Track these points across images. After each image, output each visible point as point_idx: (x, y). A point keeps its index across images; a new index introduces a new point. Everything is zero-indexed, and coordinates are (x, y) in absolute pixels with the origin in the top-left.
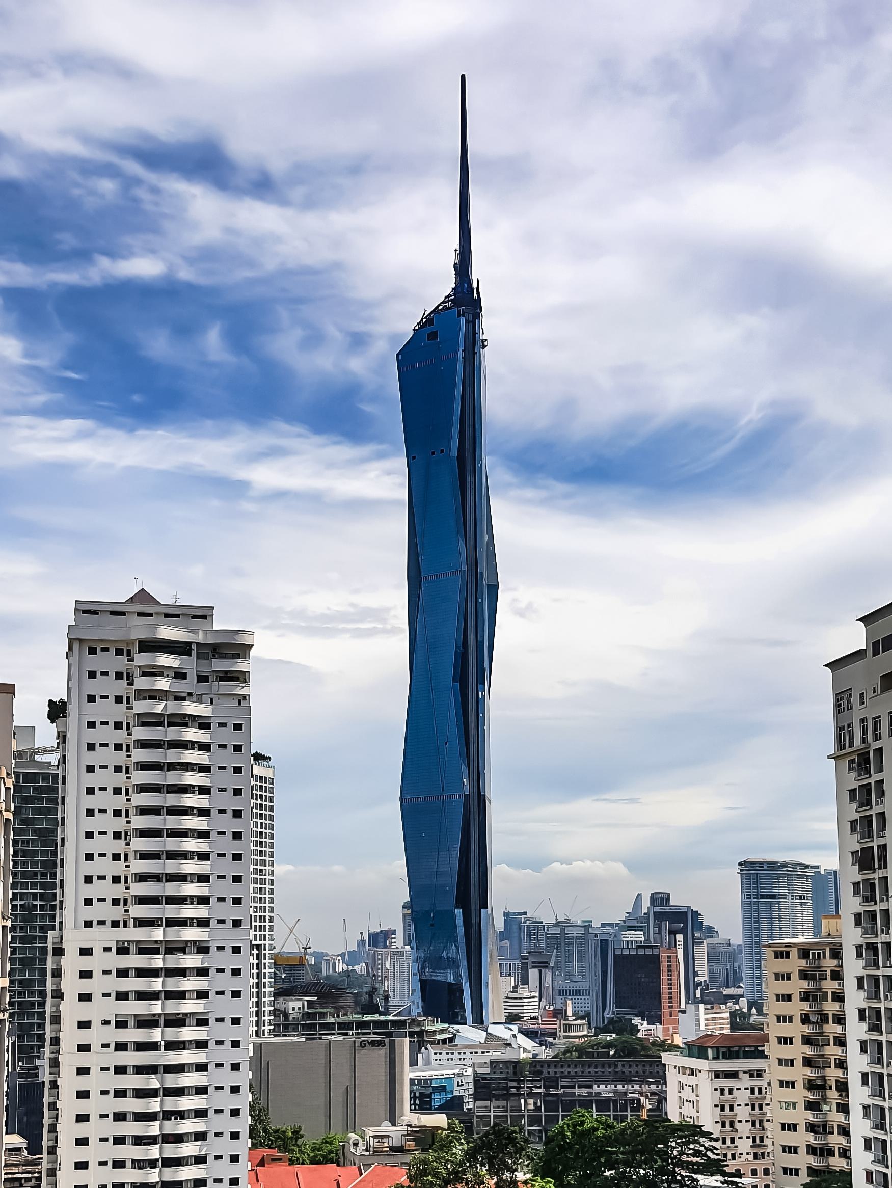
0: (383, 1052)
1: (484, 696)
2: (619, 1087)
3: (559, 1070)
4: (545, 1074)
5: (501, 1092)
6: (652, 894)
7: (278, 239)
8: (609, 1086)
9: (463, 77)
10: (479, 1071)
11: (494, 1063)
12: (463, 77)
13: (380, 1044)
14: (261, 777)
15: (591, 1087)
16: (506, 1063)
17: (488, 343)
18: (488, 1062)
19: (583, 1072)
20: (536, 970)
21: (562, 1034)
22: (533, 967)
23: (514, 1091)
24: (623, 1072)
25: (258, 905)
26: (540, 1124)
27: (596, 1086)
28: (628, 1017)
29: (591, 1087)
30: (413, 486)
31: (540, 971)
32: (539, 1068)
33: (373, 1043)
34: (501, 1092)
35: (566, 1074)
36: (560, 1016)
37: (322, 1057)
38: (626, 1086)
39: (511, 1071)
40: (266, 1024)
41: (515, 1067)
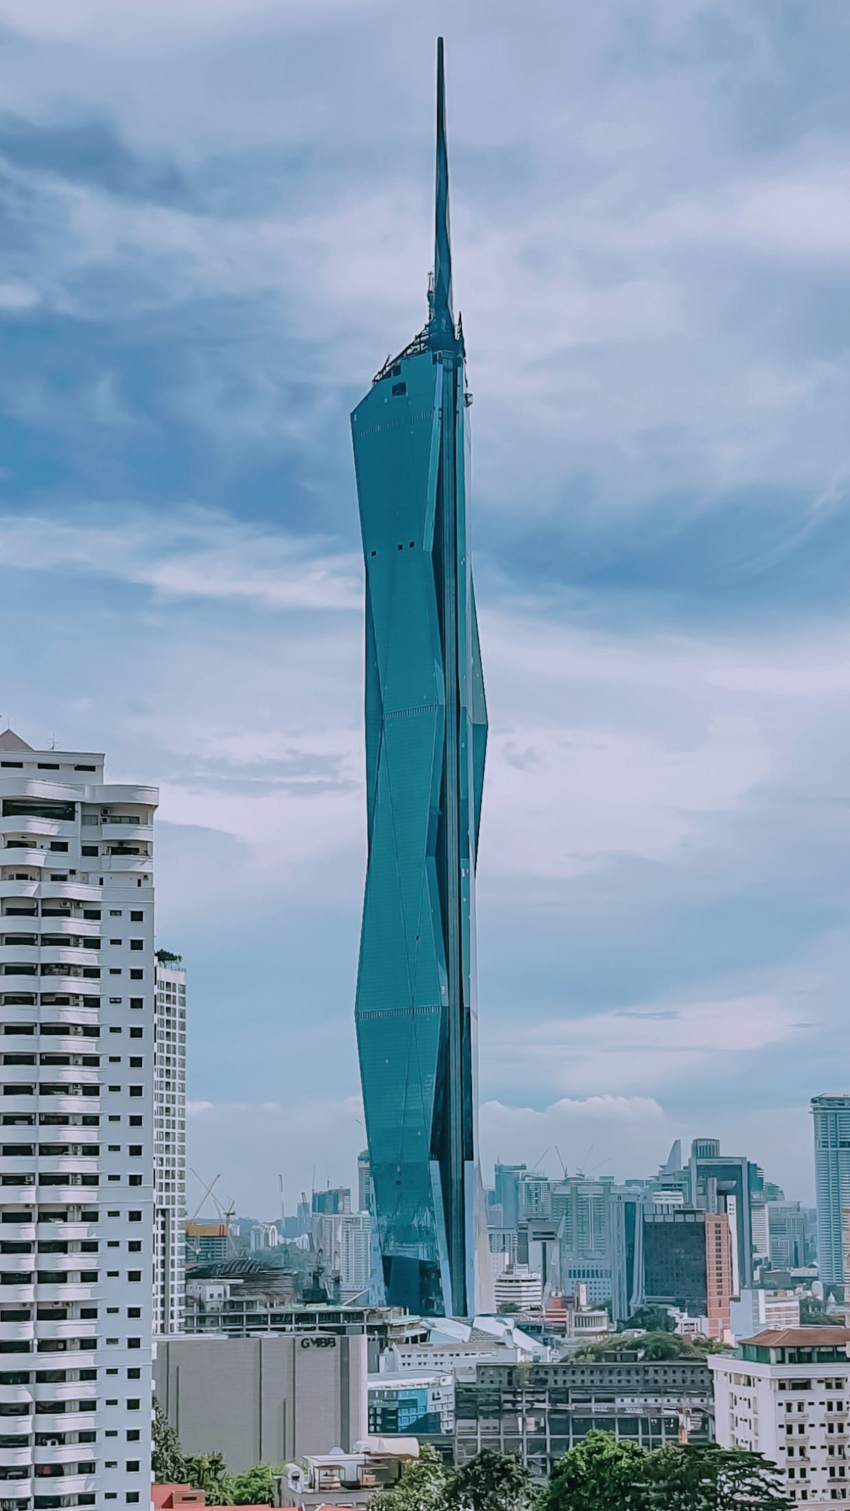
1: (468, 875)
2: (651, 1401)
5: (491, 1408)
6: (696, 1141)
10: (462, 1379)
11: (481, 1369)
13: (328, 1342)
14: (168, 984)
15: (612, 1401)
21: (574, 1329)
24: (656, 1381)
27: (618, 1400)
31: (544, 1245)
32: (542, 1375)
33: (318, 1342)
34: (491, 1408)
35: (579, 1383)
36: (570, 1305)
38: (660, 1400)
39: (505, 1379)
41: (510, 1374)
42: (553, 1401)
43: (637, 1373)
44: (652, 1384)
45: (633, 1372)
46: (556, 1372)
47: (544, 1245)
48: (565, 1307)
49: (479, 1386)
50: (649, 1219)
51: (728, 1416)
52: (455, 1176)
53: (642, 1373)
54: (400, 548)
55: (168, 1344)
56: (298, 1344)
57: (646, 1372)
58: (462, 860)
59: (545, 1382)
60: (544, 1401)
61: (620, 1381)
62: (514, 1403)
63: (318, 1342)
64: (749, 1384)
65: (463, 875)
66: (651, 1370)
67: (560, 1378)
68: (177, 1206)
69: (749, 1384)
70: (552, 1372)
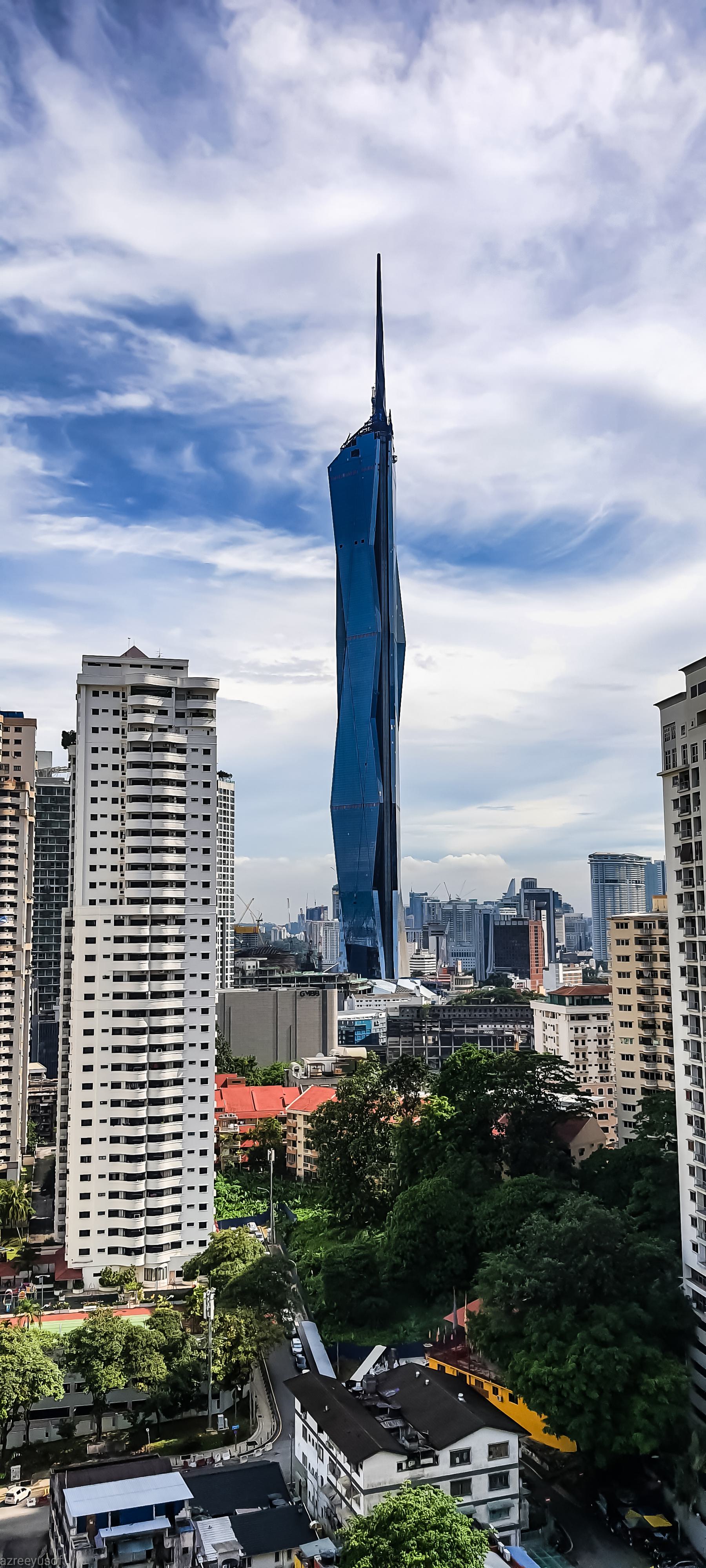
0: (318, 1000)
1: (394, 728)
4: (441, 1017)
5: (408, 1031)
6: (523, 879)
10: (391, 1014)
11: (402, 1009)
16: (412, 1008)
20: (435, 937)
21: (455, 986)
23: (417, 1029)
26: (437, 1055)
29: (476, 1026)
30: (340, 565)
31: (437, 938)
32: (436, 1012)
33: (310, 993)
34: (408, 1031)
39: (415, 1014)
44: (499, 1017)
51: (542, 1036)
68: (229, 916)
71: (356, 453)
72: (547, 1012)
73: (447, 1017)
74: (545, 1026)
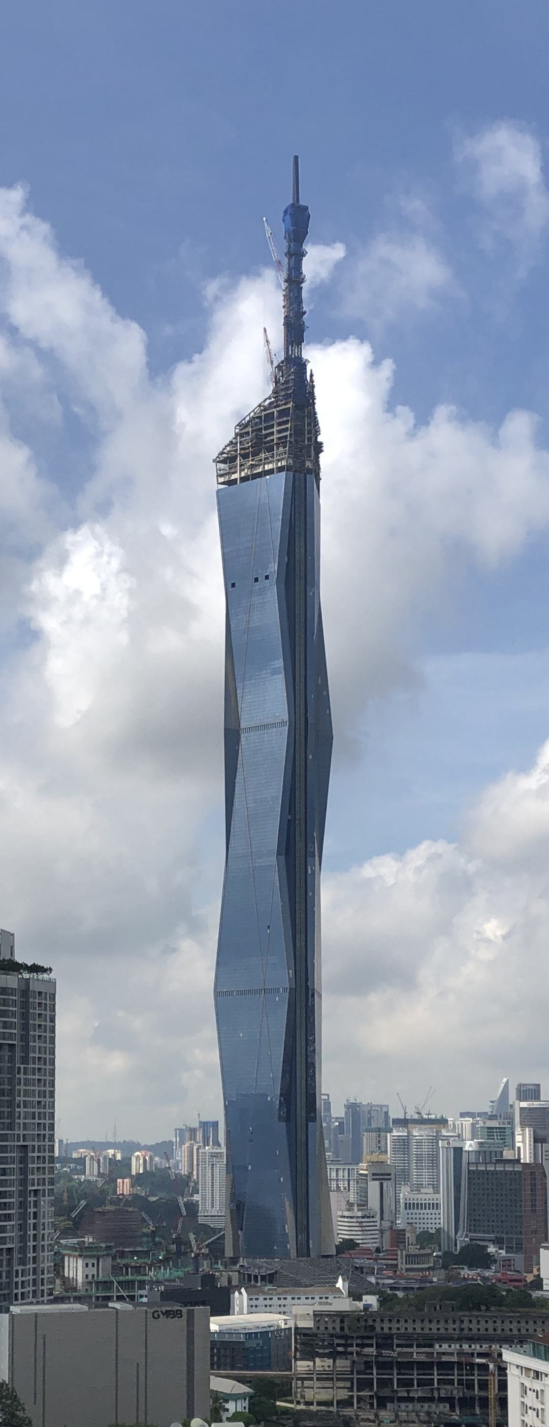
0: (183, 1321)
1: (313, 872)
2: (465, 1347)
3: (395, 1325)
4: (378, 1330)
5: (327, 1351)
6: (520, 1085)
7: (59, 575)
8: (453, 1346)
9: (296, 158)
10: (301, 1324)
11: (317, 1316)
12: (296, 158)
13: (178, 1314)
14: (40, 993)
15: (431, 1346)
16: (330, 1315)
17: (325, 448)
18: (311, 1313)
19: (422, 1329)
20: (377, 1183)
21: (404, 1266)
22: (373, 1180)
23: (340, 1349)
24: (470, 1329)
25: (36, 1110)
26: (371, 1389)
27: (437, 1346)
28: (482, 1243)
29: (431, 1346)
30: (231, 611)
31: (381, 1185)
32: (370, 1323)
33: (167, 1314)
34: (327, 1351)
35: (402, 1331)
36: (401, 1246)
37: (232, 626)
38: (473, 1346)
39: (338, 1326)
40: (46, 1272)
41: (342, 1321)
42: (378, 1346)
43: (454, 1322)
44: (466, 1332)
45: (450, 1322)
46: (382, 1321)
47: (381, 1185)
48: (398, 1246)
49: (315, 1330)
50: (472, 1168)
51: (519, 1404)
52: (301, 1137)
53: (458, 1323)
54: (256, 580)
55: (36, 1315)
56: (150, 1316)
57: (462, 1321)
58: (309, 859)
59: (373, 1328)
60: (372, 1346)
61: (438, 1329)
62: (345, 1346)
63: (167, 1314)
64: (538, 1378)
65: (310, 872)
66: (466, 1319)
67: (386, 1326)
68: (47, 1187)
69: (538, 1378)
70: (378, 1320)
71: (233, 585)
72: (528, 1369)
73: (386, 1331)
74: (524, 1390)
